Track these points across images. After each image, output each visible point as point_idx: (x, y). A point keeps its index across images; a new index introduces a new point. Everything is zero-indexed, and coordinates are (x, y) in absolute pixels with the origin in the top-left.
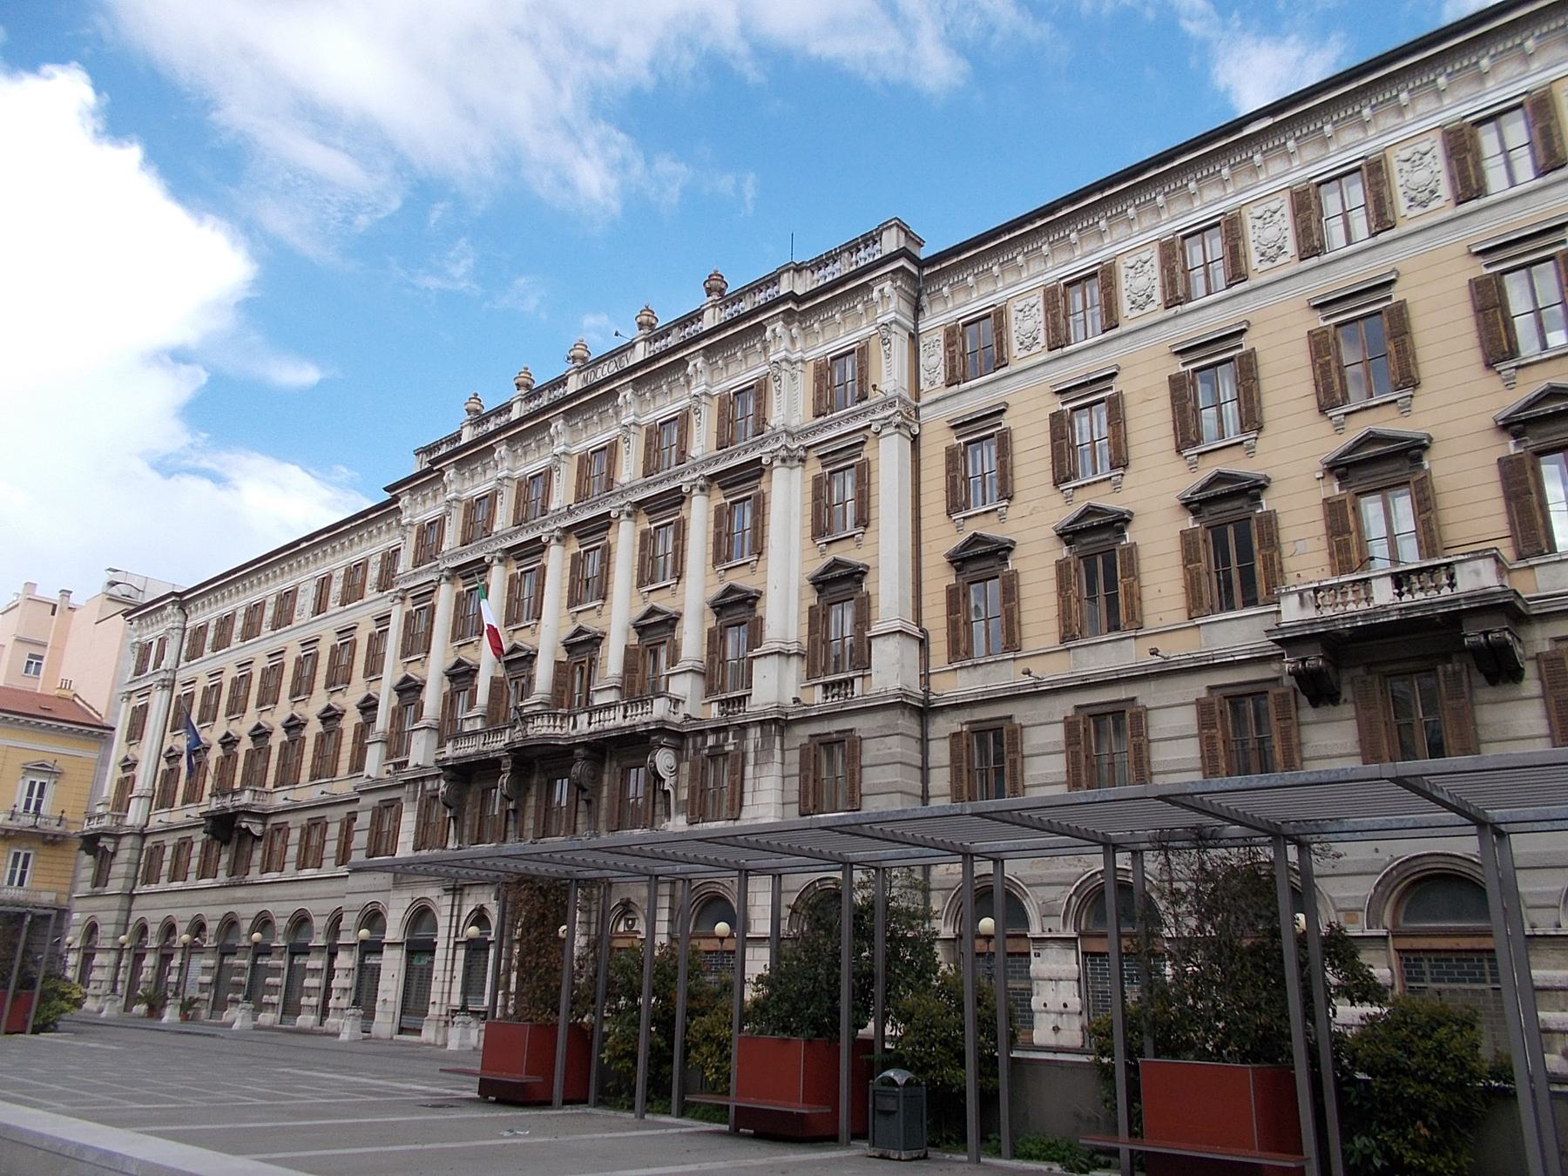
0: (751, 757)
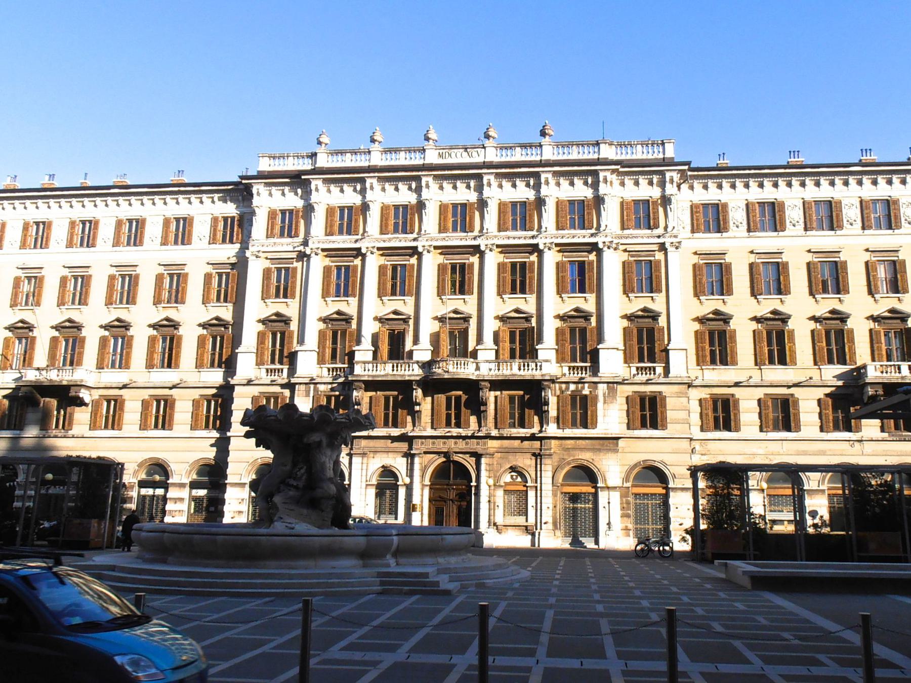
0: (601, 398)
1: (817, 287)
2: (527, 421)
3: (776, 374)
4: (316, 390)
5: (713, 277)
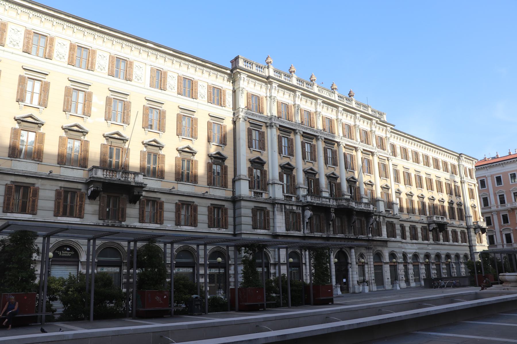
2: (271, 224)
4: (285, 208)
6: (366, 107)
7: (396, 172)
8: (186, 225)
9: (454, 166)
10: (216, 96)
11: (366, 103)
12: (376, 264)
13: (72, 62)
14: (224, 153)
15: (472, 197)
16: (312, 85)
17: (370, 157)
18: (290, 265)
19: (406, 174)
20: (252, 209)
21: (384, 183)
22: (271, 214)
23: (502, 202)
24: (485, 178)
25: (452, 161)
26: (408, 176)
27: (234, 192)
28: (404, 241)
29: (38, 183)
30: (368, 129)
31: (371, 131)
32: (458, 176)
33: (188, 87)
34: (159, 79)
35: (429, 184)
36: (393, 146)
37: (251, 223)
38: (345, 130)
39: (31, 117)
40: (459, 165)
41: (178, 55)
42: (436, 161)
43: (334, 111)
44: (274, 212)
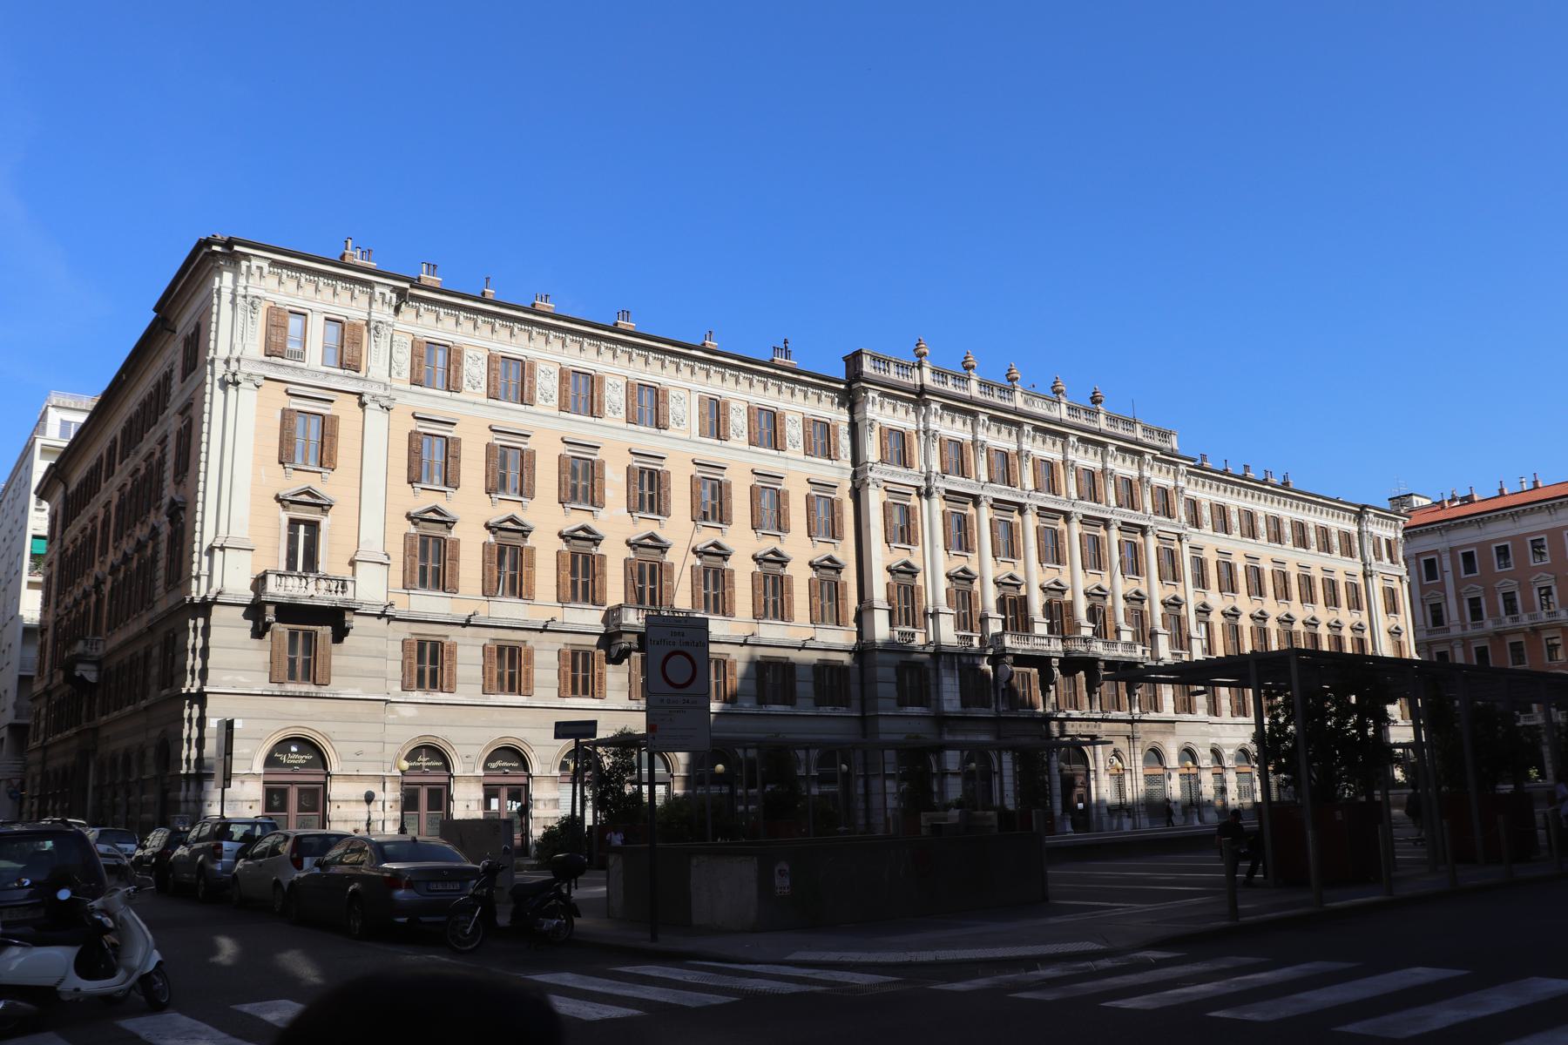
1: (496, 485)
2: (933, 696)
3: (508, 609)
4: (960, 662)
5: (430, 457)
6: (1165, 435)
7: (1200, 564)
8: (912, 705)
9: (1346, 537)
10: (820, 439)
11: (1129, 416)
12: (1149, 772)
13: (566, 405)
14: (838, 557)
15: (1392, 608)
16: (1012, 391)
17: (1139, 539)
18: (968, 776)
19: (1223, 567)
20: (897, 668)
21: (1168, 592)
22: (932, 674)
23: (1476, 613)
24: (1422, 559)
25: (1340, 524)
26: (1256, 574)
27: (860, 634)
28: (1213, 719)
29: (455, 634)
30: (1012, 446)
31: (1141, 478)
32: (1358, 559)
33: (768, 430)
34: (715, 419)
35: (1280, 584)
36: (1193, 505)
37: (895, 694)
38: (1082, 484)
39: (435, 510)
40: (1360, 533)
41: (746, 366)
42: (1300, 527)
43: (1059, 444)
44: (937, 670)
